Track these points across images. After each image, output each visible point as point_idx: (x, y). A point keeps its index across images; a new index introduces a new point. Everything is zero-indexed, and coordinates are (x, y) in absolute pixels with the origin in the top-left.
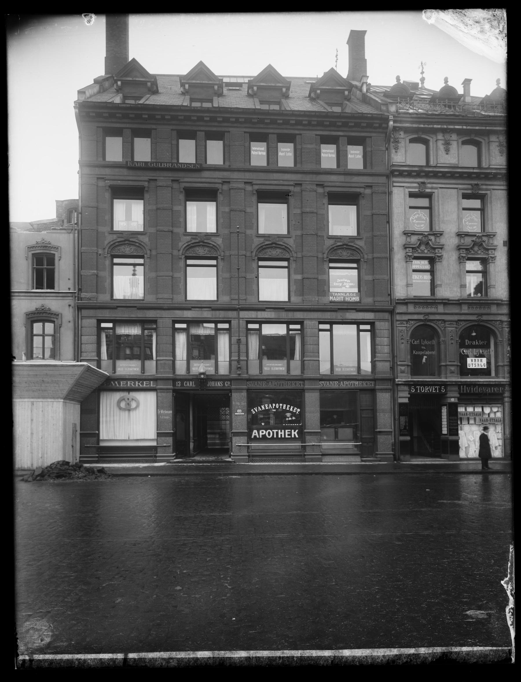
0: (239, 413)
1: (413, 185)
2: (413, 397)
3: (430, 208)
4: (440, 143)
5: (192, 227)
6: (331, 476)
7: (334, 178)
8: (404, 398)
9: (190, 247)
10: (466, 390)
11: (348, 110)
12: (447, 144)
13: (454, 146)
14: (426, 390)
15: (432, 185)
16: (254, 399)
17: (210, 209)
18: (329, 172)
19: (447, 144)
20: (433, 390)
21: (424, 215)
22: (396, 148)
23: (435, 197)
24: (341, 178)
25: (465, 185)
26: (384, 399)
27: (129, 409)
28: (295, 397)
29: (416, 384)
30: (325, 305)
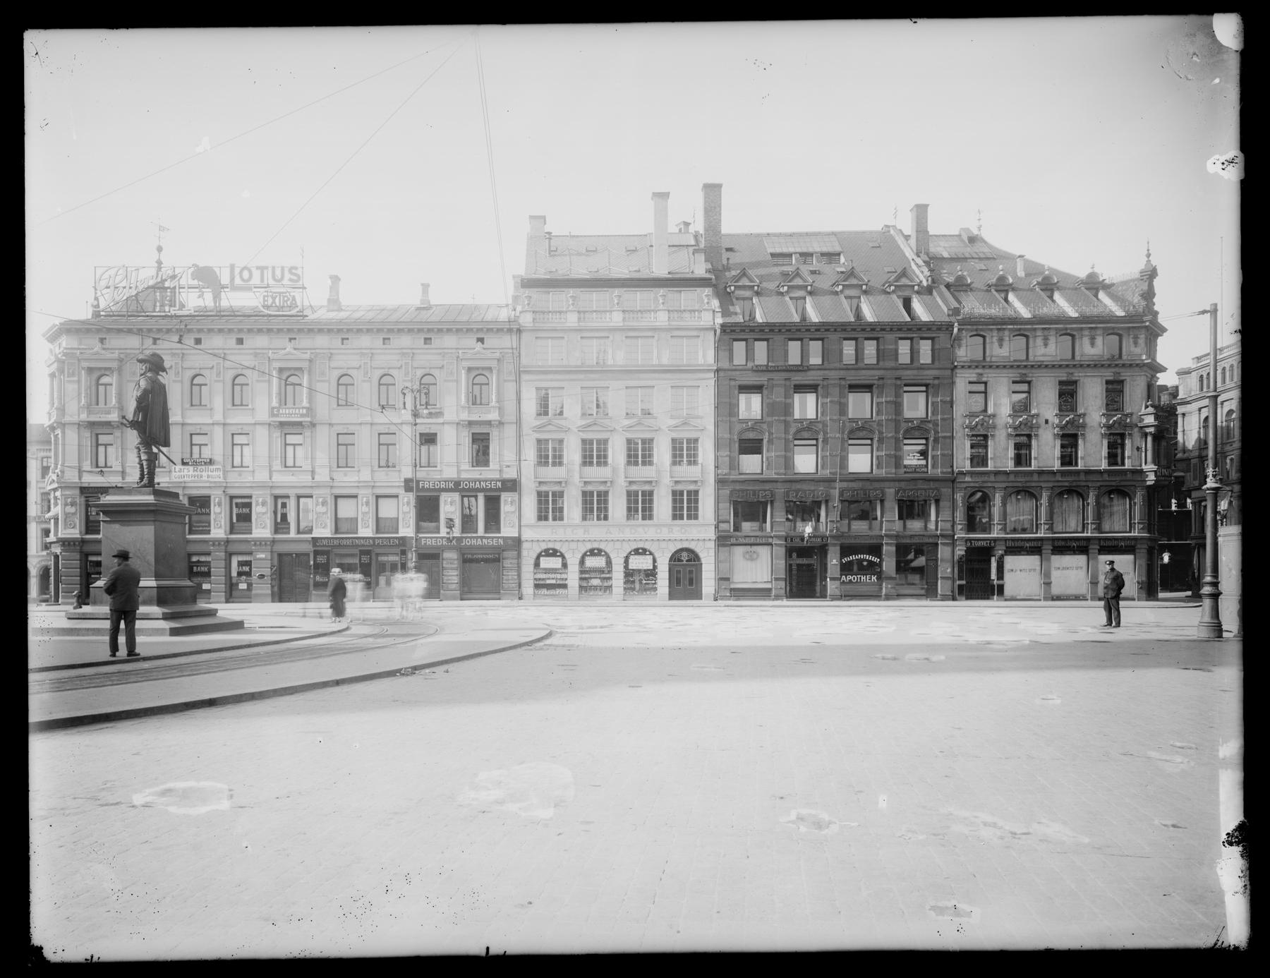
0: (833, 561)
1: (972, 375)
2: (968, 550)
3: (985, 393)
4: (995, 339)
5: (743, 414)
6: (456, 664)
7: (909, 372)
8: (960, 551)
9: (799, 431)
10: (1010, 544)
11: (224, 303)
12: (1046, 339)
13: (1052, 340)
14: (979, 544)
15: (989, 375)
16: (846, 550)
17: (811, 399)
18: (905, 367)
19: (1046, 339)
20: (984, 544)
21: (980, 398)
22: (960, 346)
23: (1033, 384)
24: (915, 372)
25: (1014, 374)
26: (943, 552)
27: (752, 559)
28: (876, 549)
29: (970, 540)
30: (915, 472)
